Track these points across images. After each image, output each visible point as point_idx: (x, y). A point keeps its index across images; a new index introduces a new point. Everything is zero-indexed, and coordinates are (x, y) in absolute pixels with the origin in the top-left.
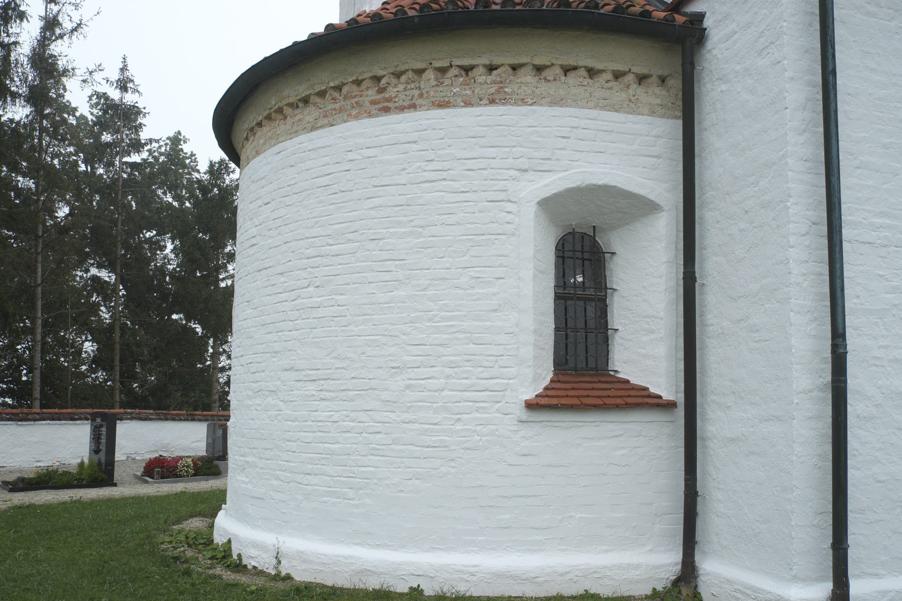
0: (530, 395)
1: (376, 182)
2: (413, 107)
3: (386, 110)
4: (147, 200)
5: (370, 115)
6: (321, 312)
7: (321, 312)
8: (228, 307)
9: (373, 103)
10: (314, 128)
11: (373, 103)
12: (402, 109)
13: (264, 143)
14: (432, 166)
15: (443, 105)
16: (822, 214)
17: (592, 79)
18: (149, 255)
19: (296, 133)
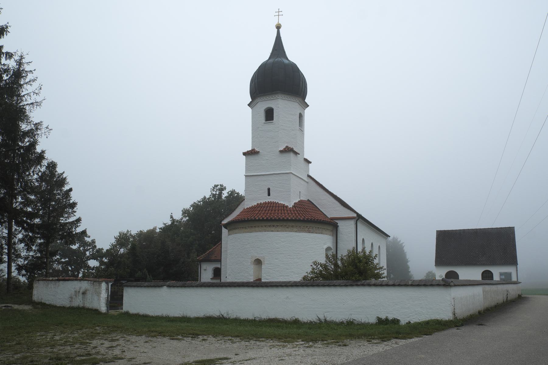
0: (211, 278)
1: (308, 243)
2: (313, 233)
3: (309, 232)
4: (74, 222)
5: (307, 233)
6: (299, 263)
7: (299, 263)
8: (514, 247)
9: (307, 231)
10: (296, 232)
11: (307, 231)
12: (312, 233)
13: (280, 230)
14: (315, 242)
15: (316, 233)
16: (338, 244)
17: (254, 261)
18: (16, 155)
19: (292, 232)
